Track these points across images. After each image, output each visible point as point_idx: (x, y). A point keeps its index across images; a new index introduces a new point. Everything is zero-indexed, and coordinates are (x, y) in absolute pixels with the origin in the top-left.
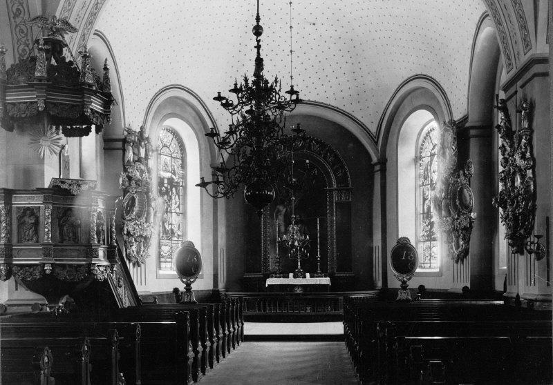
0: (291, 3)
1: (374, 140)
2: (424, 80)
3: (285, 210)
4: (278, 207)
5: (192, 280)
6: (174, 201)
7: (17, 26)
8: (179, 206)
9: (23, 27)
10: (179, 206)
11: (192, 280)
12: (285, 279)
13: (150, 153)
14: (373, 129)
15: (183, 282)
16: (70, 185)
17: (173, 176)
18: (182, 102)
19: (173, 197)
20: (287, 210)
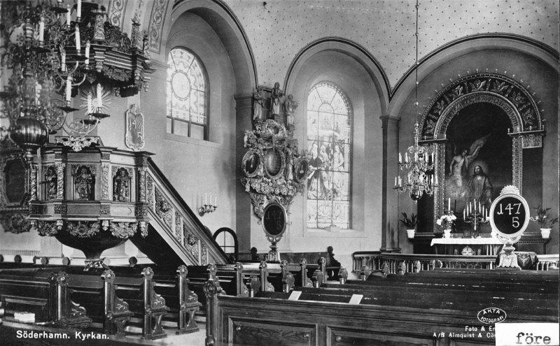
0: (265, 3)
1: (389, 94)
2: (498, 39)
3: (463, 161)
4: (455, 158)
5: (277, 239)
6: (336, 160)
7: (120, 10)
8: (343, 165)
9: (116, 6)
10: (343, 165)
11: (277, 239)
12: (487, 239)
13: (291, 110)
14: (393, 84)
15: (270, 240)
16: (73, 142)
17: (336, 134)
18: (352, 59)
19: (336, 155)
20: (464, 162)
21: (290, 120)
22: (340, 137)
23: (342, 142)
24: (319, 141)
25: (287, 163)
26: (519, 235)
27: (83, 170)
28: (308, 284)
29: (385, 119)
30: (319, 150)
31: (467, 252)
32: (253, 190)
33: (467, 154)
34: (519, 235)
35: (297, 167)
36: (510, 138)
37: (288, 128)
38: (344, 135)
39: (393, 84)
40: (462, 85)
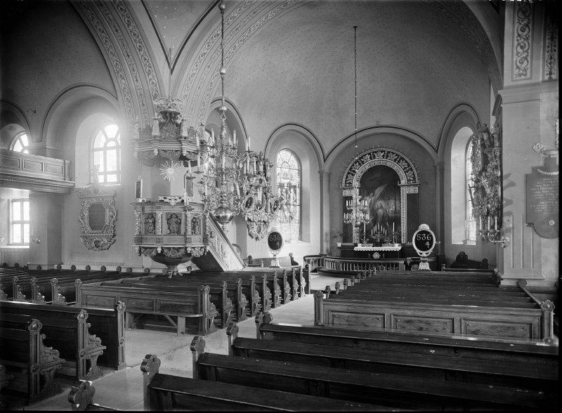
6: (292, 198)
8: (296, 201)
21: (268, 174)
22: (294, 183)
23: (295, 187)
24: (281, 186)
25: (267, 202)
26: (430, 251)
27: (174, 216)
28: (228, 303)
29: (321, 173)
30: (281, 191)
31: (376, 256)
32: (249, 220)
33: (373, 196)
34: (430, 251)
35: (273, 203)
36: (399, 188)
37: (267, 180)
38: (296, 182)
39: (326, 152)
40: (369, 154)
